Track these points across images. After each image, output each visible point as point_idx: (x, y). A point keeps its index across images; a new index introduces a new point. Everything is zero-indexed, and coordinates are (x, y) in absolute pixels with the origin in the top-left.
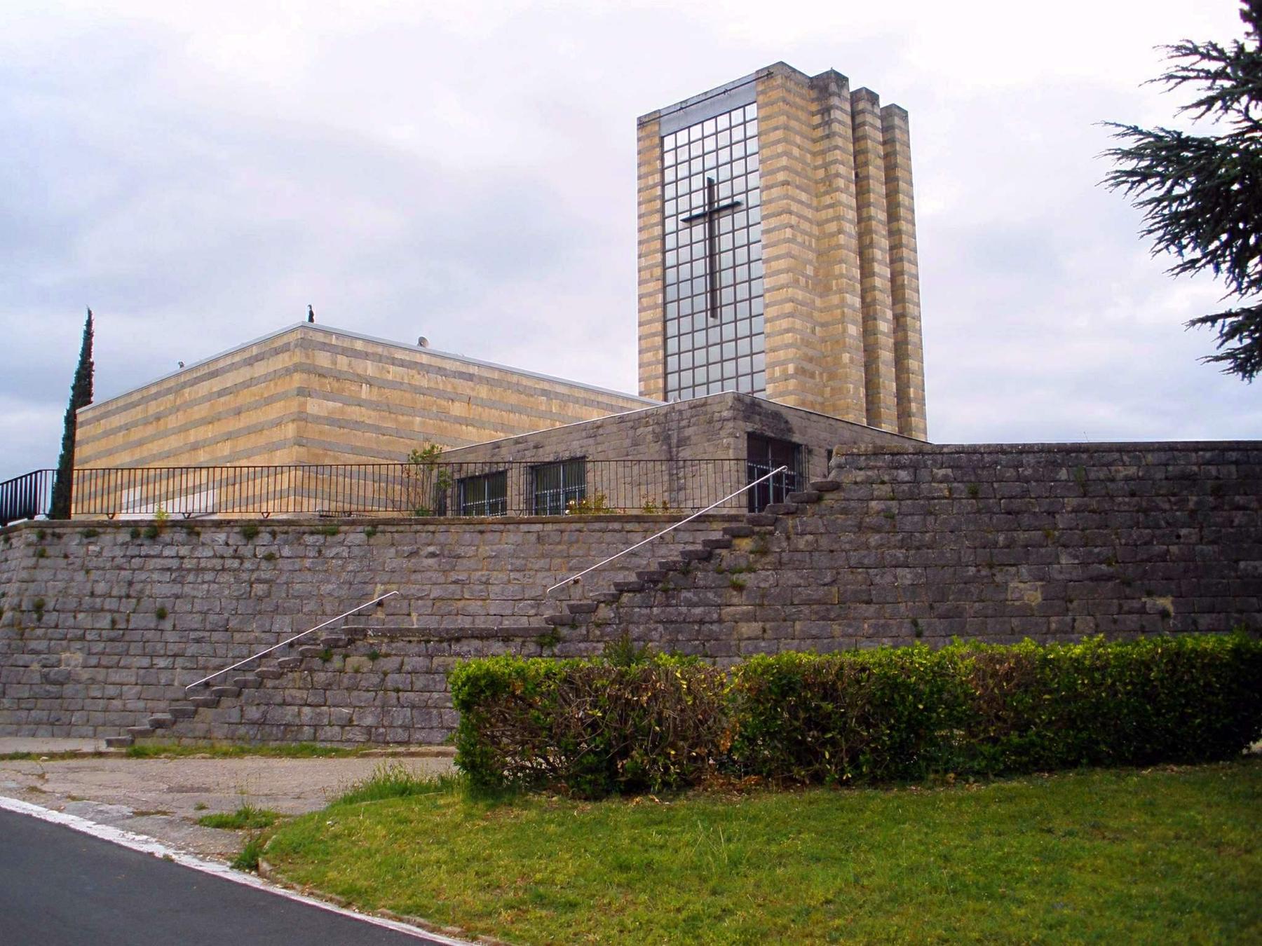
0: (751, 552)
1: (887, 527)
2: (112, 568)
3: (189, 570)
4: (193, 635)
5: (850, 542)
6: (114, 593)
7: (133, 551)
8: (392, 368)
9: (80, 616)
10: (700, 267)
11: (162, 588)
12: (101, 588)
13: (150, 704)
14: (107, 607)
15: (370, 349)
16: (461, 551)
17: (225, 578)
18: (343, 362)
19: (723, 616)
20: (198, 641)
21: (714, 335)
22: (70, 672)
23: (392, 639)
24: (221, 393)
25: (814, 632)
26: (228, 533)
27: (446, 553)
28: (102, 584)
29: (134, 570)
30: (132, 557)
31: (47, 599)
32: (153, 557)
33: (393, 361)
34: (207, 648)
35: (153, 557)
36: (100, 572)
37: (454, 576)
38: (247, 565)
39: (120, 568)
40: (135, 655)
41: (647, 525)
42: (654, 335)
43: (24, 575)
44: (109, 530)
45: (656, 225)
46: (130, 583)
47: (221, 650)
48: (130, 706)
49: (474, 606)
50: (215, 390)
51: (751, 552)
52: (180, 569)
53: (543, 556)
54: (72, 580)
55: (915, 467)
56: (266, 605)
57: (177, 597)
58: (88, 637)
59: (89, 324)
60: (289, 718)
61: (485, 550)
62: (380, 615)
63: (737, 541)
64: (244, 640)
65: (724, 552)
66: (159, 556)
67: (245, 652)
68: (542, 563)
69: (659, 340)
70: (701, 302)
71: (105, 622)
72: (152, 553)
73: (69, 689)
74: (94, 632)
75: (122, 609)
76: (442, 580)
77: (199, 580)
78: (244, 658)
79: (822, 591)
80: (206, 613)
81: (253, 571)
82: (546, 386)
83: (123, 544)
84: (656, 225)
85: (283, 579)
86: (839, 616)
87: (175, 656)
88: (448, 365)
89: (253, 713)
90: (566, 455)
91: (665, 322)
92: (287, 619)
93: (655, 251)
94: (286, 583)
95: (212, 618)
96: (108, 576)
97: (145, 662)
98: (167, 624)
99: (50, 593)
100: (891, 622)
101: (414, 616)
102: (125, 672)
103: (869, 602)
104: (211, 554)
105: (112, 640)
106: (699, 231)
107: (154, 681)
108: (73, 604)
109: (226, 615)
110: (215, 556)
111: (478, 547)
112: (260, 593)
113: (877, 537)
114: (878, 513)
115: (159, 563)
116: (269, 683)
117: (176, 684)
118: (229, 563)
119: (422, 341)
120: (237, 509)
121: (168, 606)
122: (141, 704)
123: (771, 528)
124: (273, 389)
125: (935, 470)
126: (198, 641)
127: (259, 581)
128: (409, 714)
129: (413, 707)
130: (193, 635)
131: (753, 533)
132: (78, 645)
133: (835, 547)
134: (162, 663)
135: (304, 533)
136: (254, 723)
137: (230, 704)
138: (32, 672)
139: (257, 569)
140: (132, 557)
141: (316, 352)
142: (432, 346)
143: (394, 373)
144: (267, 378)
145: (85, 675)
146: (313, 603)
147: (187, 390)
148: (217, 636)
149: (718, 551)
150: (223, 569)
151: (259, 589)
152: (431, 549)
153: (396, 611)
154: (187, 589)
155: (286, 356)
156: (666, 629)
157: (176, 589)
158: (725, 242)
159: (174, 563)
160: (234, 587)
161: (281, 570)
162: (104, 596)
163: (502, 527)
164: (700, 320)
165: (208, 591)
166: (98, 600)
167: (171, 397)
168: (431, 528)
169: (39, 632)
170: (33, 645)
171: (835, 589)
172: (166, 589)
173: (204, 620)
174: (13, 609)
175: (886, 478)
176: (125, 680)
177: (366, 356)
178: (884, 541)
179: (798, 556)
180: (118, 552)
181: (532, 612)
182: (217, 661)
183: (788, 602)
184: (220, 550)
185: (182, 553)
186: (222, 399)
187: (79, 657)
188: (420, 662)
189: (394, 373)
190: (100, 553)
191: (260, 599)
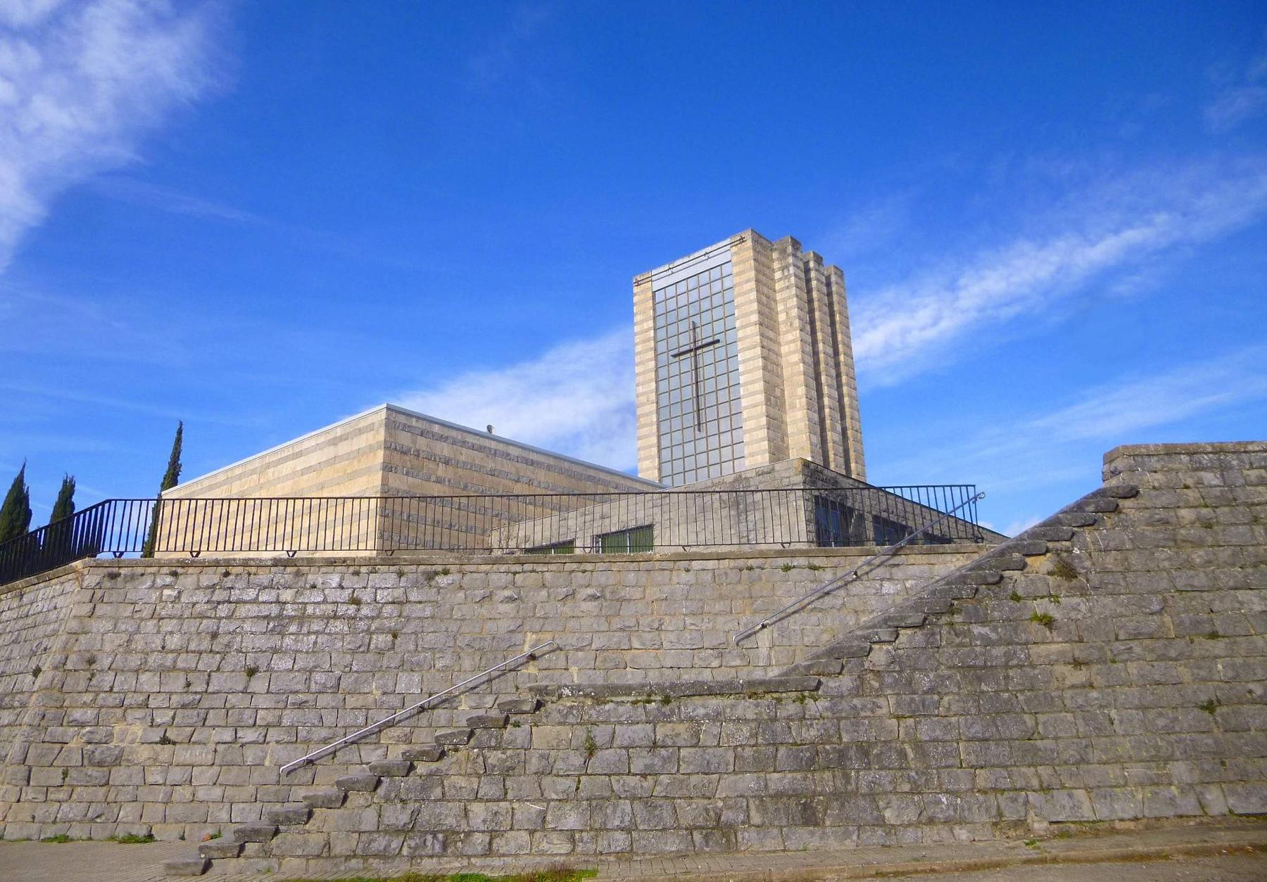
0: (1050, 573)
1: (1210, 540)
2: (191, 617)
3: (291, 618)
4: (292, 699)
5: (1169, 559)
6: (193, 646)
7: (219, 595)
8: (464, 450)
9: (144, 677)
10: (689, 392)
11: (254, 639)
12: (174, 642)
13: (230, 792)
14: (180, 664)
15: (446, 432)
16: (624, 593)
17: (339, 626)
18: (422, 443)
19: (1034, 658)
20: (301, 705)
21: (702, 446)
22: (122, 750)
23: (599, 700)
24: (304, 471)
25: (1157, 677)
26: (343, 574)
27: (608, 595)
28: (176, 637)
29: (220, 619)
30: (219, 603)
31: (99, 656)
32: (245, 602)
33: (464, 443)
34: (311, 716)
35: (245, 602)
36: (175, 621)
37: (616, 623)
38: (365, 611)
39: (202, 617)
40: (214, 727)
41: (836, 560)
42: (651, 446)
43: (73, 625)
44: (191, 570)
45: (650, 360)
46: (214, 636)
47: (329, 719)
48: (201, 795)
49: (647, 658)
50: (299, 468)
51: (1050, 573)
52: (280, 616)
53: (721, 597)
54: (138, 631)
55: (1223, 468)
56: (391, 660)
57: (275, 651)
58: (152, 703)
59: (180, 432)
60: (450, 821)
61: (653, 593)
62: (532, 669)
63: (1029, 560)
64: (359, 704)
65: (1016, 574)
66: (255, 601)
67: (361, 720)
68: (719, 606)
69: (655, 450)
70: (690, 420)
71: (177, 683)
72: (246, 598)
73: (119, 775)
74: (161, 697)
75: (200, 667)
76: (604, 627)
77: (305, 630)
78: (360, 727)
79: (1153, 622)
80: (311, 672)
81: (373, 618)
82: (592, 473)
83: (208, 587)
84: (650, 360)
85: (409, 629)
86: (1181, 654)
87: (268, 726)
88: (514, 452)
89: (397, 816)
90: (632, 525)
91: (659, 437)
92: (416, 677)
93: (650, 381)
94: (415, 633)
95: (318, 677)
96: (185, 627)
97: (228, 735)
98: (259, 684)
99: (107, 648)
100: (1251, 660)
101: (574, 669)
102: (198, 749)
103: (1214, 635)
104: (320, 599)
105: (184, 707)
106: (687, 364)
107: (239, 760)
108: (134, 661)
109: (338, 673)
110: (325, 601)
111: (645, 588)
112: (382, 645)
113: (1201, 552)
114: (1193, 523)
115: (253, 610)
116: (422, 768)
117: (267, 763)
118: (342, 610)
119: (489, 428)
120: (354, 547)
121: (262, 662)
122: (217, 792)
123: (1068, 544)
124: (356, 466)
125: (1246, 472)
126: (301, 705)
127: (380, 631)
128: (628, 809)
129: (633, 798)
130: (292, 699)
131: (1048, 551)
132: (140, 713)
133: (1152, 565)
134: (249, 735)
135: (436, 573)
136: (398, 831)
137: (362, 801)
138: (70, 750)
139: (378, 616)
140: (219, 603)
141: (398, 432)
142: (495, 432)
143: (465, 455)
144: (348, 456)
145: (144, 753)
146: (449, 656)
147: (271, 470)
148: (324, 700)
149: (1007, 573)
150: (335, 617)
151: (381, 640)
152: (590, 591)
153: (552, 665)
154: (288, 641)
155: (370, 435)
156: (964, 676)
157: (275, 641)
158: (708, 372)
159: (275, 610)
160: (348, 638)
161: (408, 618)
162: (178, 652)
163: (671, 565)
164: (689, 434)
165: (315, 643)
166: (171, 656)
167: (255, 477)
168: (589, 567)
169: (88, 698)
170: (77, 714)
171: (1167, 619)
172: (263, 642)
173: (308, 680)
174: (56, 668)
175: (1190, 482)
176: (198, 760)
177: (442, 438)
178: (1212, 557)
179: (1108, 578)
180: (201, 597)
181: (715, 663)
182: (324, 733)
183: (1112, 637)
184: (333, 595)
185: (282, 598)
186: (306, 477)
187: (138, 730)
188: (640, 732)
189: (465, 455)
190: (179, 596)
191: (380, 652)
